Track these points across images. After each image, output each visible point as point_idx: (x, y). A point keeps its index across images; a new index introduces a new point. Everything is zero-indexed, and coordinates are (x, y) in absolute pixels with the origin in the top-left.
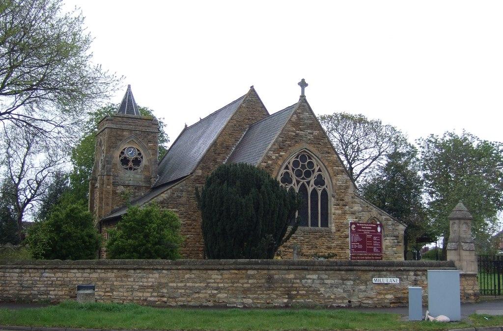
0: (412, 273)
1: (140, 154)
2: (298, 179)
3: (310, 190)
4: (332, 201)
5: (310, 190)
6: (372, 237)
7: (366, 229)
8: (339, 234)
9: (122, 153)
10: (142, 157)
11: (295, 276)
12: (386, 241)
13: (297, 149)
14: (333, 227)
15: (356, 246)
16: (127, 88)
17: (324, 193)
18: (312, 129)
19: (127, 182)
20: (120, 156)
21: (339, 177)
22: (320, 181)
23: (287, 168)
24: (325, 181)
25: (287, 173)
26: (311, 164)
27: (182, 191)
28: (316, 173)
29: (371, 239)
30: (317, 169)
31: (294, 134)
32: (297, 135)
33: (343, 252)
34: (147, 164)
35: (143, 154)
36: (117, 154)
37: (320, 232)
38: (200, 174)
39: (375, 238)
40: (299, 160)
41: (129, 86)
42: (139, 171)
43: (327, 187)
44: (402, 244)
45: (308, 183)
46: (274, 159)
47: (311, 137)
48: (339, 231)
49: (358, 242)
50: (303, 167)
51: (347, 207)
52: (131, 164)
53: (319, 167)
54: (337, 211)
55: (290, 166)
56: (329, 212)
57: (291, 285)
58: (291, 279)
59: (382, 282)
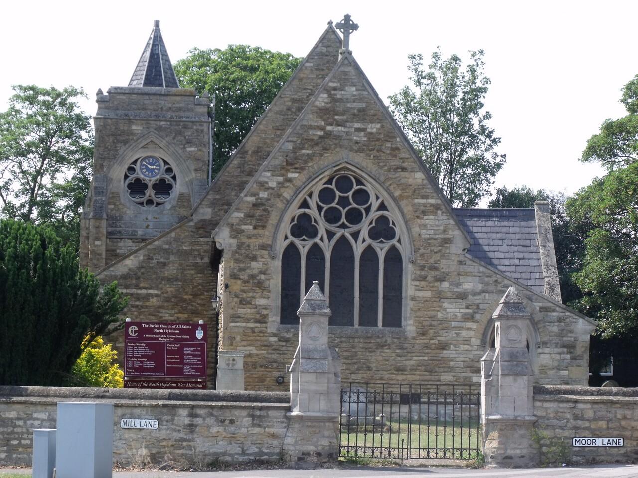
0: (184, 412)
1: (169, 170)
2: (332, 227)
3: (358, 249)
4: (409, 271)
5: (358, 249)
6: (181, 349)
7: (166, 334)
8: (421, 341)
9: (131, 169)
10: (174, 178)
11: (18, 414)
12: (542, 356)
13: (328, 163)
14: (410, 326)
15: (137, 365)
16: (152, 27)
17: (394, 257)
18: (363, 120)
19: (140, 232)
20: (126, 177)
21: (429, 219)
22: (383, 230)
23: (305, 204)
24: (397, 229)
25: (305, 217)
26: (361, 196)
27: (167, 251)
28: (374, 214)
29: (180, 351)
30: (375, 204)
31: (321, 133)
32: (328, 135)
33: (433, 378)
34: (185, 190)
35: (176, 170)
36: (118, 172)
37: (378, 337)
38: (208, 217)
39: (187, 350)
40: (333, 186)
41: (157, 24)
42: (168, 206)
43: (399, 241)
44: (585, 362)
45: (356, 235)
46: (273, 189)
47: (362, 137)
48: (423, 334)
49: (143, 356)
50: (344, 202)
51: (445, 285)
52: (150, 192)
53: (380, 201)
54: (420, 294)
55: (313, 202)
56: (403, 295)
57: (12, 429)
58: (12, 419)
59: (134, 427)
